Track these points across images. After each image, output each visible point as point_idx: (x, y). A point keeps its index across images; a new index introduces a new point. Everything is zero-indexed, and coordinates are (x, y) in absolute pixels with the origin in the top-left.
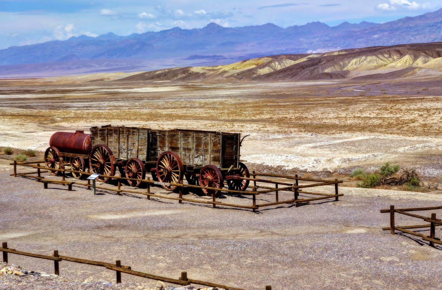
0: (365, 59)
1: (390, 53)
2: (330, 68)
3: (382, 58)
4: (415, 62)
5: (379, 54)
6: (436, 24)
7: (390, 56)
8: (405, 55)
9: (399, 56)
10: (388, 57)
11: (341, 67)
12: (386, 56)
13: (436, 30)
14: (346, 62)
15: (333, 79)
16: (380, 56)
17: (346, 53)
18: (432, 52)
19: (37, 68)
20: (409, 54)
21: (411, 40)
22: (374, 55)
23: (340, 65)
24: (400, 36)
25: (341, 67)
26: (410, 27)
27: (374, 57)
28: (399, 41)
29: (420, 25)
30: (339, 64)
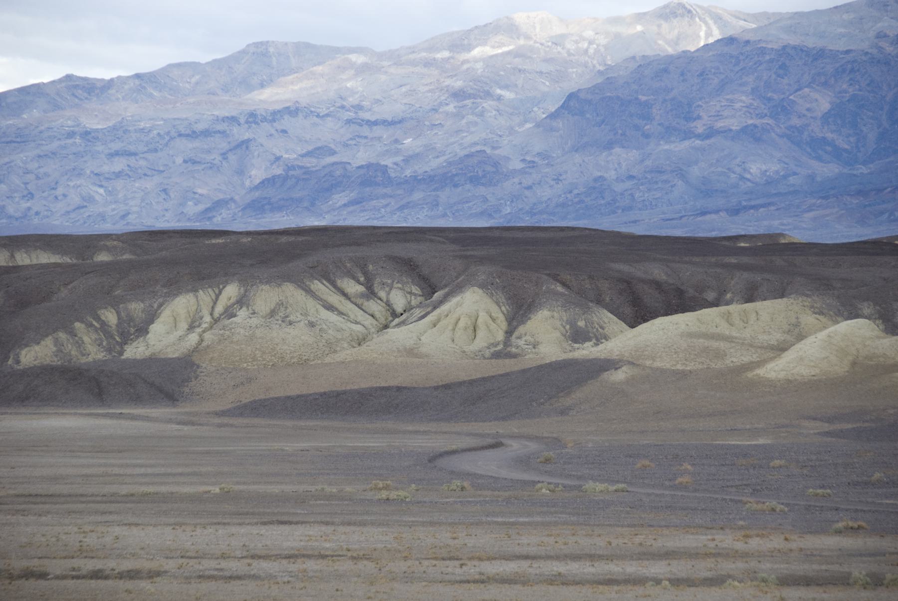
0: (242, 302)
1: (365, 274)
2: (49, 342)
3: (334, 299)
4: (521, 329)
5: (313, 277)
6: (220, 127)
7: (371, 293)
8: (458, 289)
9: (416, 290)
10: (362, 296)
11: (109, 335)
12: (353, 288)
13: (224, 155)
14: (136, 308)
15: (109, 406)
16: (318, 286)
17: (67, 260)
18: (591, 277)
19: (56, 265)
20: (482, 286)
21: (90, 199)
22: (288, 278)
23: (104, 324)
24: (31, 177)
25: (109, 335)
26: (86, 134)
27: (291, 292)
28: (25, 205)
29: (142, 125)
30: (98, 318)
